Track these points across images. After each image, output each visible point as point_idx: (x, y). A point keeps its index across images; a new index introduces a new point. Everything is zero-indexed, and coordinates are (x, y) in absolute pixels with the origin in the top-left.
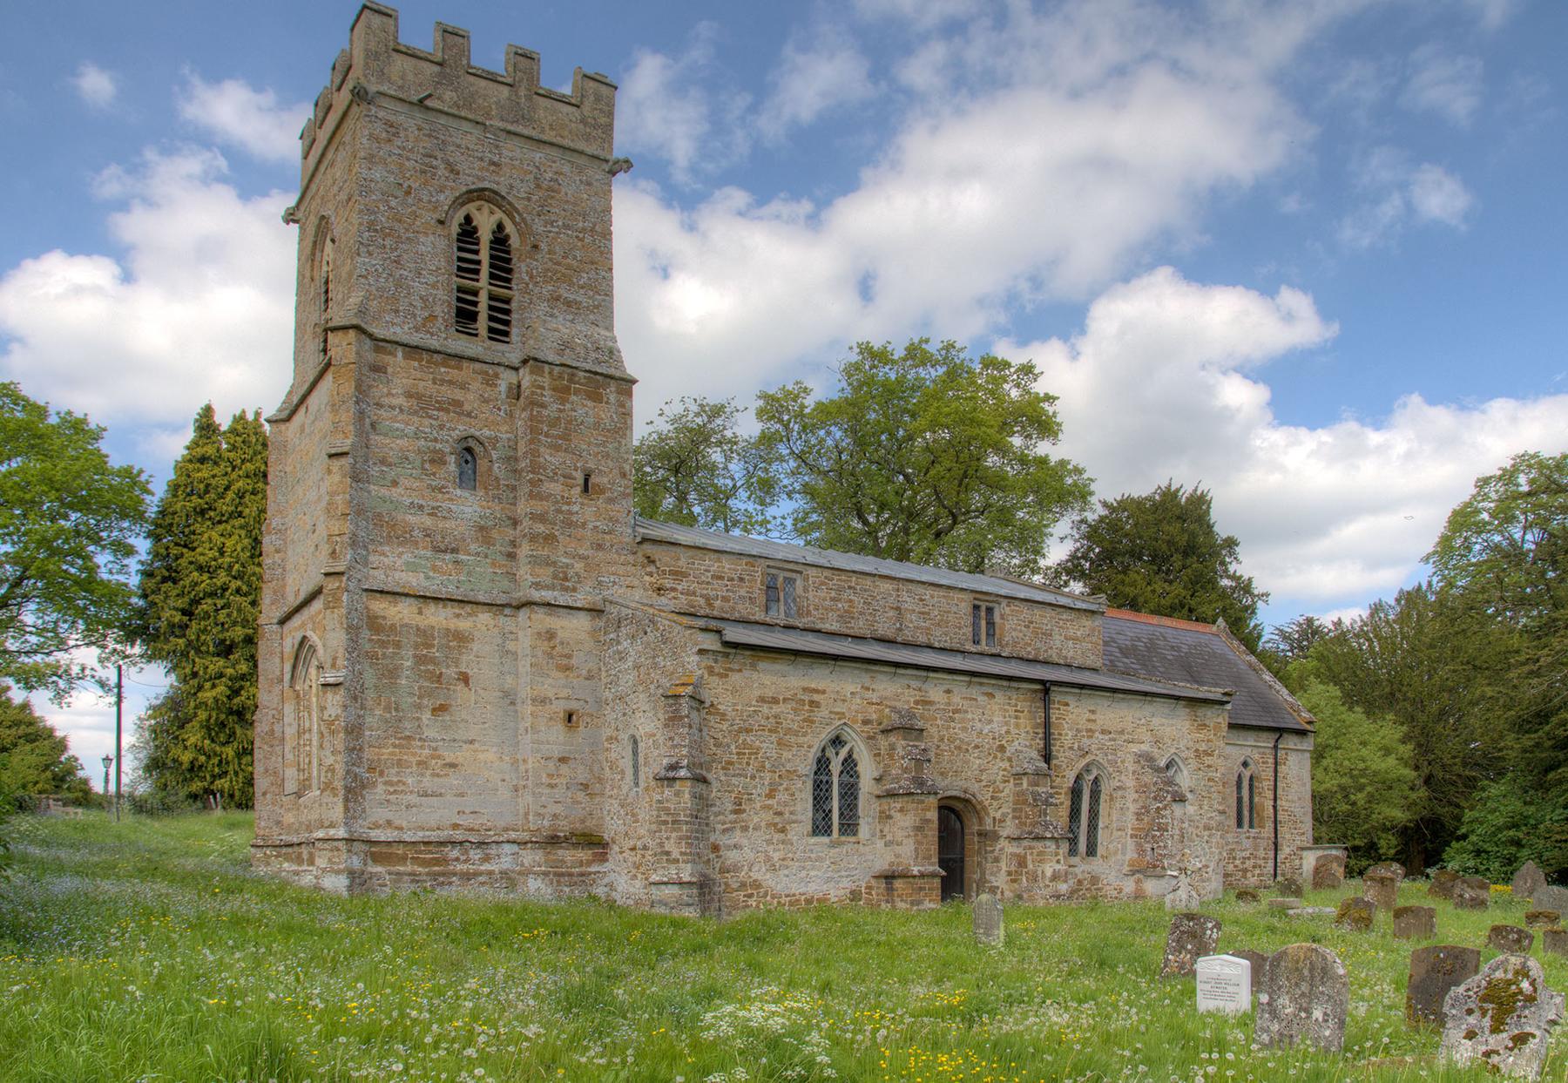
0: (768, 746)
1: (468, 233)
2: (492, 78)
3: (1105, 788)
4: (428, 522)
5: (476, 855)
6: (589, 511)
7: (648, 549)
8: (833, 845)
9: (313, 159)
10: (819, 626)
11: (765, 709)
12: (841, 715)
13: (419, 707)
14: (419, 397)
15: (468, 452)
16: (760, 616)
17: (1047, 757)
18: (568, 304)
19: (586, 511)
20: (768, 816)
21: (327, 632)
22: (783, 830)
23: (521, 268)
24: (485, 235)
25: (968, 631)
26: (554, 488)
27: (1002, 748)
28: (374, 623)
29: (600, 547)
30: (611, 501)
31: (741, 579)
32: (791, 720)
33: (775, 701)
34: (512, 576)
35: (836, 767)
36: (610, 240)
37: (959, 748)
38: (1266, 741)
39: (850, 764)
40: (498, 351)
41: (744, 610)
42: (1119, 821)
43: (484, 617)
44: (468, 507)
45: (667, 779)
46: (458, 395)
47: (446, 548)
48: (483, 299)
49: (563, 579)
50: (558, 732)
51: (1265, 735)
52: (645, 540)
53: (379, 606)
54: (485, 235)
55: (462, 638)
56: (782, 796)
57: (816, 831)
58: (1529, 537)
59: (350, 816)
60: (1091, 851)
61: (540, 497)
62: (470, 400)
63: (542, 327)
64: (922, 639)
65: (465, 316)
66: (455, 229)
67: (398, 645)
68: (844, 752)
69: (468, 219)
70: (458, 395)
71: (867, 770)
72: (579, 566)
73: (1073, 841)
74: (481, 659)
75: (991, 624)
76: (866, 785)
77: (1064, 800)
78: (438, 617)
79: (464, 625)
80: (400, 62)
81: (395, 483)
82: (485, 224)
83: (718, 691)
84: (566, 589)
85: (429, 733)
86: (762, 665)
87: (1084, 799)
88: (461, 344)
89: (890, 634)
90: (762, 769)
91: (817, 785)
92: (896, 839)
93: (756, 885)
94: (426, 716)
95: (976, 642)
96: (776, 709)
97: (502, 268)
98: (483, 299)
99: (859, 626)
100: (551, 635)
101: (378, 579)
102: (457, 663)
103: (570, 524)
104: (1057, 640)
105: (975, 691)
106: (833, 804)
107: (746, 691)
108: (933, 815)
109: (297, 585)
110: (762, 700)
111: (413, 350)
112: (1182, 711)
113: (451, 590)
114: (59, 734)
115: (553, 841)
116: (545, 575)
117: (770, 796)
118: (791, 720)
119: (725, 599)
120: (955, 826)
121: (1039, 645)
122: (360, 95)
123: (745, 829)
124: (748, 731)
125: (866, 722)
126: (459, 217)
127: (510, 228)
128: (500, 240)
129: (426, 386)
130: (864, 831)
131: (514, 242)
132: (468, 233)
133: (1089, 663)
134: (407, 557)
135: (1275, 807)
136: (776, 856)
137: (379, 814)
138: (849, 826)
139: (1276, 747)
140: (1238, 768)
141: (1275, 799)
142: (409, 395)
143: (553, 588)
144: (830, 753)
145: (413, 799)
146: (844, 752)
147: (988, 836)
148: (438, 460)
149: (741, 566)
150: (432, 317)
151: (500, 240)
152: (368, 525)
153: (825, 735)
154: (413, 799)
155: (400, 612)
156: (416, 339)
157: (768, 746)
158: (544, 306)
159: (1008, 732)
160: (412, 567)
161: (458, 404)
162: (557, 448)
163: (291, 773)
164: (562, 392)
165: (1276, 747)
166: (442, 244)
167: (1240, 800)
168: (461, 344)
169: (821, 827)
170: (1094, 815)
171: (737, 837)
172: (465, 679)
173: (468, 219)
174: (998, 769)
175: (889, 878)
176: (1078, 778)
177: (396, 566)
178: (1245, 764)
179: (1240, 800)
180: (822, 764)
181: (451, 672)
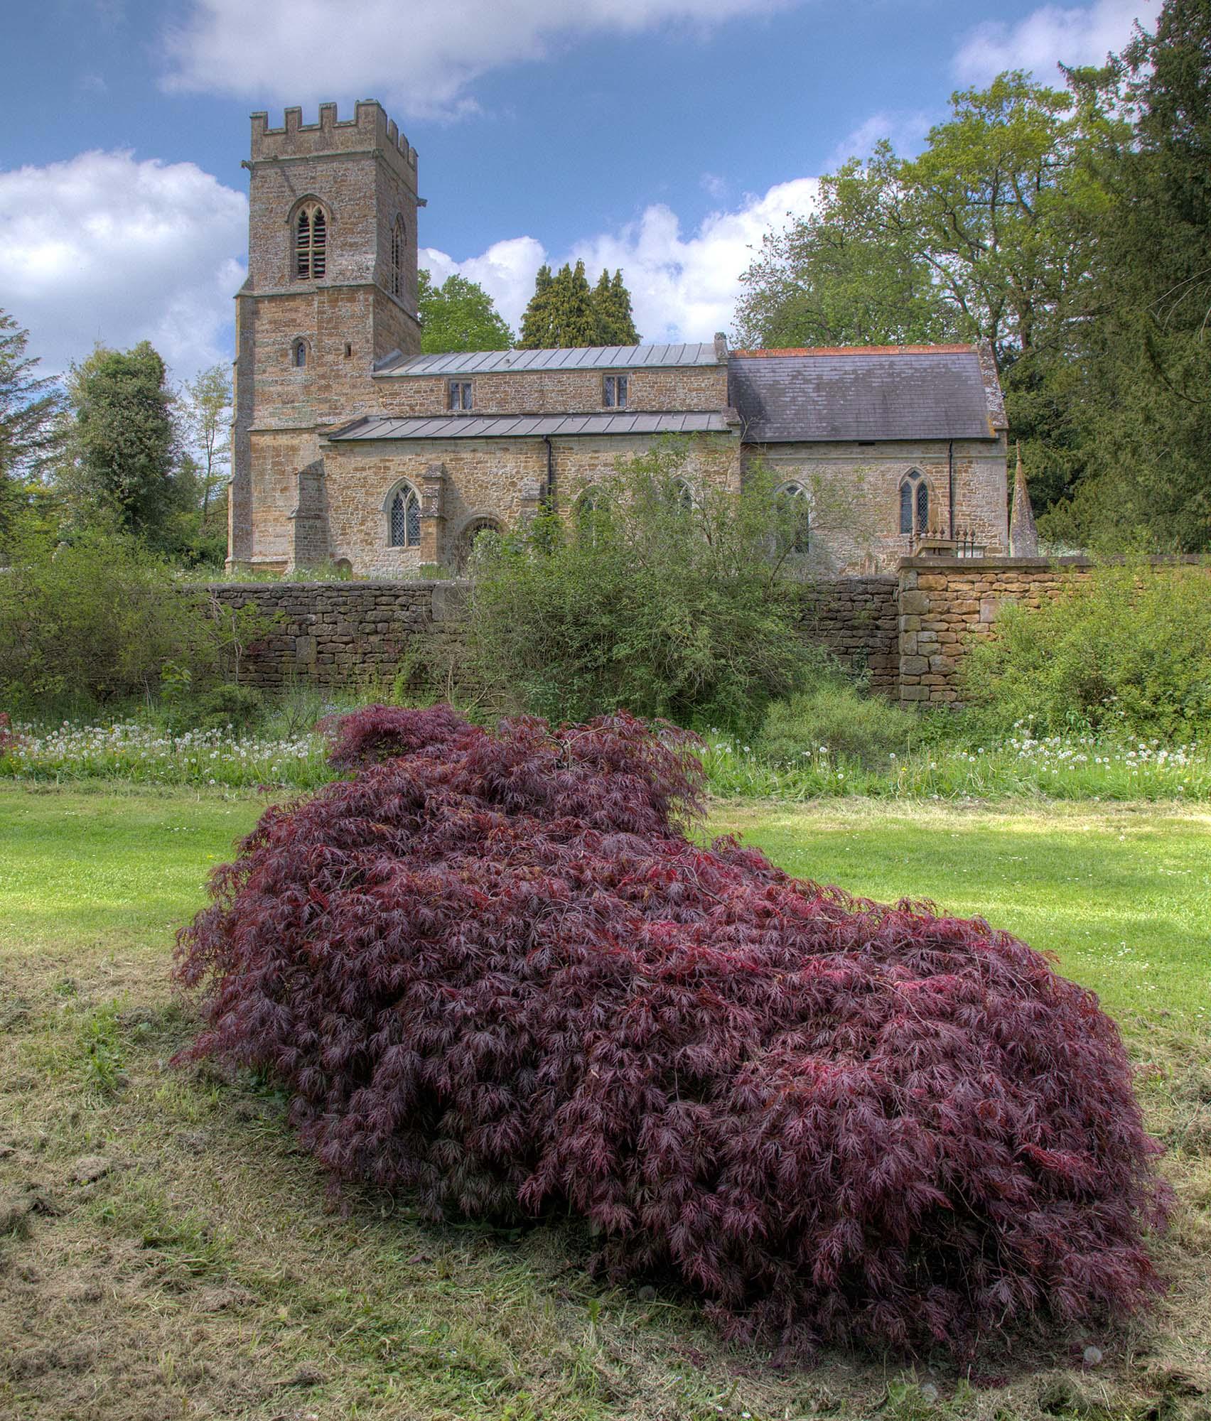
0: (360, 495)
4: (279, 388)
6: (348, 367)
8: (402, 552)
10: (484, 411)
11: (358, 475)
12: (404, 473)
13: (274, 489)
14: (275, 322)
16: (443, 411)
18: (351, 245)
19: (347, 367)
20: (362, 536)
22: (371, 544)
23: (329, 230)
24: (311, 220)
25: (599, 398)
26: (330, 358)
27: (513, 484)
29: (354, 386)
30: (360, 358)
31: (432, 390)
32: (373, 479)
33: (363, 469)
37: (480, 486)
39: (413, 500)
43: (306, 436)
44: (299, 375)
46: (294, 315)
47: (288, 401)
51: (937, 447)
54: (311, 220)
55: (294, 449)
56: (370, 524)
58: (15, 431)
61: (322, 365)
62: (299, 316)
64: (560, 409)
67: (264, 458)
70: (294, 315)
72: (343, 400)
78: (284, 440)
79: (296, 442)
81: (264, 372)
82: (311, 214)
83: (331, 467)
84: (336, 414)
85: (280, 503)
86: (356, 450)
89: (535, 409)
90: (357, 509)
91: (394, 516)
94: (278, 494)
95: (607, 402)
96: (364, 474)
97: (320, 239)
99: (512, 408)
102: (292, 462)
103: (337, 376)
104: (681, 392)
107: (339, 469)
110: (356, 469)
111: (272, 298)
113: (291, 425)
116: (325, 408)
117: (362, 524)
118: (373, 479)
119: (421, 405)
121: (662, 399)
123: (349, 544)
124: (348, 488)
125: (417, 476)
126: (299, 214)
127: (324, 212)
128: (319, 219)
129: (279, 316)
133: (712, 407)
134: (271, 410)
135: (951, 513)
136: (367, 559)
139: (951, 457)
141: (951, 505)
142: (270, 323)
143: (329, 414)
144: (402, 496)
145: (272, 539)
148: (285, 355)
149: (432, 383)
150: (283, 276)
151: (319, 219)
154: (272, 539)
156: (275, 291)
157: (360, 495)
158: (339, 251)
159: (518, 472)
160: (272, 415)
161: (294, 320)
162: (331, 335)
165: (951, 457)
166: (288, 233)
168: (300, 286)
169: (395, 540)
173: (304, 213)
178: (914, 474)
181: (289, 469)
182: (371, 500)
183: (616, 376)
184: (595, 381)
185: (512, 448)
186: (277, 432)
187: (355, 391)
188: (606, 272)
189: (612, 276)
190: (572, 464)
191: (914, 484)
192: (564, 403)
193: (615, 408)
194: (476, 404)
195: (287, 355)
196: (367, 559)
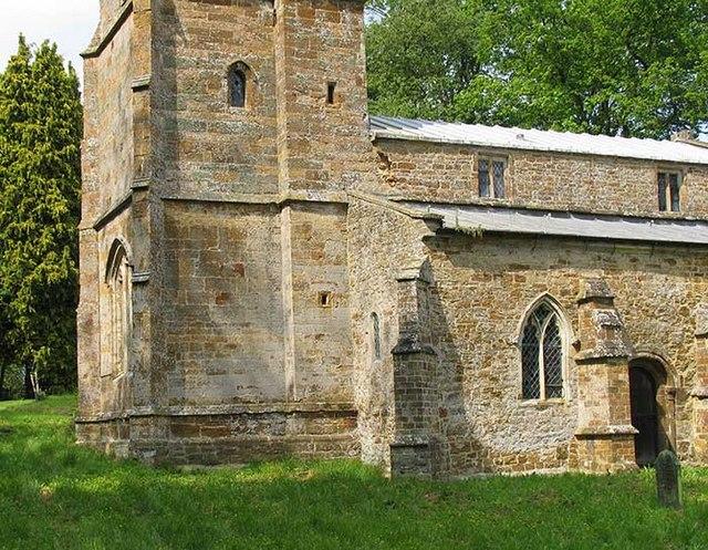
4: (209, 137)
5: (252, 424)
16: (475, 198)
20: (485, 383)
22: (498, 395)
50: (315, 312)
56: (497, 364)
62: (237, 29)
64: (614, 210)
70: (228, 27)
71: (566, 336)
76: (566, 350)
84: (317, 187)
90: (478, 340)
95: (662, 208)
99: (558, 202)
100: (307, 228)
105: (656, 259)
119: (445, 186)
130: (566, 391)
138: (554, 389)
154: (203, 377)
159: (689, 295)
162: (305, 66)
180: (529, 333)
182: (499, 327)
183: (668, 173)
185: (680, 262)
186: (210, 205)
187: (344, 155)
188: (24, 51)
189: (50, 46)
192: (618, 202)
193: (669, 212)
194: (514, 192)
195: (219, 87)
196: (494, 418)
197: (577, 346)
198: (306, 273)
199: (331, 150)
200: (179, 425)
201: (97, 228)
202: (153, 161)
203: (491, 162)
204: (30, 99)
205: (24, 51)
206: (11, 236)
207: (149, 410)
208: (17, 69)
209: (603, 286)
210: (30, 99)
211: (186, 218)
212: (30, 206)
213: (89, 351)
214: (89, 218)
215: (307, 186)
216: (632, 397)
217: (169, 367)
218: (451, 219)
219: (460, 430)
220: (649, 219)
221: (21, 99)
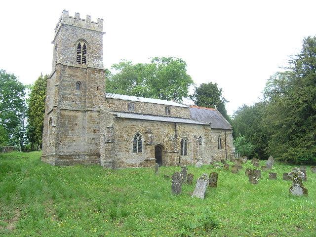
0: (125, 136)
1: (79, 46)
2: (83, 20)
3: (188, 142)
5: (77, 157)
7: (108, 100)
9: (57, 32)
10: (137, 112)
15: (79, 83)
16: (127, 111)
17: (176, 136)
21: (53, 116)
24: (82, 46)
28: (61, 115)
32: (129, 131)
34: (85, 105)
35: (138, 138)
36: (102, 48)
38: (223, 132)
40: (84, 66)
41: (122, 109)
42: (190, 148)
43: (80, 113)
45: (108, 142)
48: (81, 57)
49: (93, 106)
50: (92, 134)
52: (107, 98)
53: (63, 112)
54: (82, 46)
55: (76, 117)
57: (134, 152)
59: (56, 151)
60: (186, 155)
62: (78, 74)
63: (91, 63)
65: (78, 59)
66: (77, 46)
68: (139, 136)
69: (79, 44)
71: (143, 139)
73: (182, 153)
74: (79, 121)
75: (169, 111)
76: (143, 143)
77: (179, 146)
79: (77, 114)
80: (69, 19)
82: (82, 44)
87: (184, 143)
88: (78, 65)
92: (148, 153)
93: (123, 162)
97: (85, 53)
98: (81, 57)
99: (145, 112)
100: (91, 116)
101: (63, 107)
105: (162, 125)
106: (138, 148)
108: (154, 148)
109: (51, 108)
112: (202, 127)
114: (11, 74)
115: (90, 155)
118: (129, 131)
120: (159, 151)
122: (62, 25)
128: (84, 46)
130: (143, 151)
131: (87, 47)
132: (79, 46)
137: (62, 150)
138: (140, 151)
140: (218, 137)
142: (68, 74)
146: (139, 136)
147: (166, 152)
151: (84, 46)
152: (62, 97)
153: (135, 134)
155: (67, 113)
163: (48, 142)
164: (93, 72)
166: (75, 48)
167: (218, 143)
168: (78, 65)
170: (186, 147)
171: (120, 153)
172: (76, 124)
173: (79, 44)
174: (167, 139)
175: (146, 160)
176: (182, 140)
177: (66, 105)
178: (219, 136)
179: (218, 143)
180: (135, 139)
184: (164, 108)
187: (100, 101)
188: (42, 76)
190: (180, 129)
191: (220, 138)
197: (145, 142)
198: (90, 125)
199: (97, 100)
200: (61, 157)
201: (48, 114)
202: (59, 101)
203: (131, 104)
204: (42, 86)
205: (42, 76)
206: (36, 115)
207: (54, 154)
208: (40, 79)
209: (150, 130)
210: (42, 86)
211: (63, 112)
212: (41, 108)
213: (280, 177)
214: (46, 112)
215: (91, 107)
216: (156, 153)
217: (59, 144)
218: (119, 115)
219: (120, 159)
220: (163, 116)
221: (40, 85)
